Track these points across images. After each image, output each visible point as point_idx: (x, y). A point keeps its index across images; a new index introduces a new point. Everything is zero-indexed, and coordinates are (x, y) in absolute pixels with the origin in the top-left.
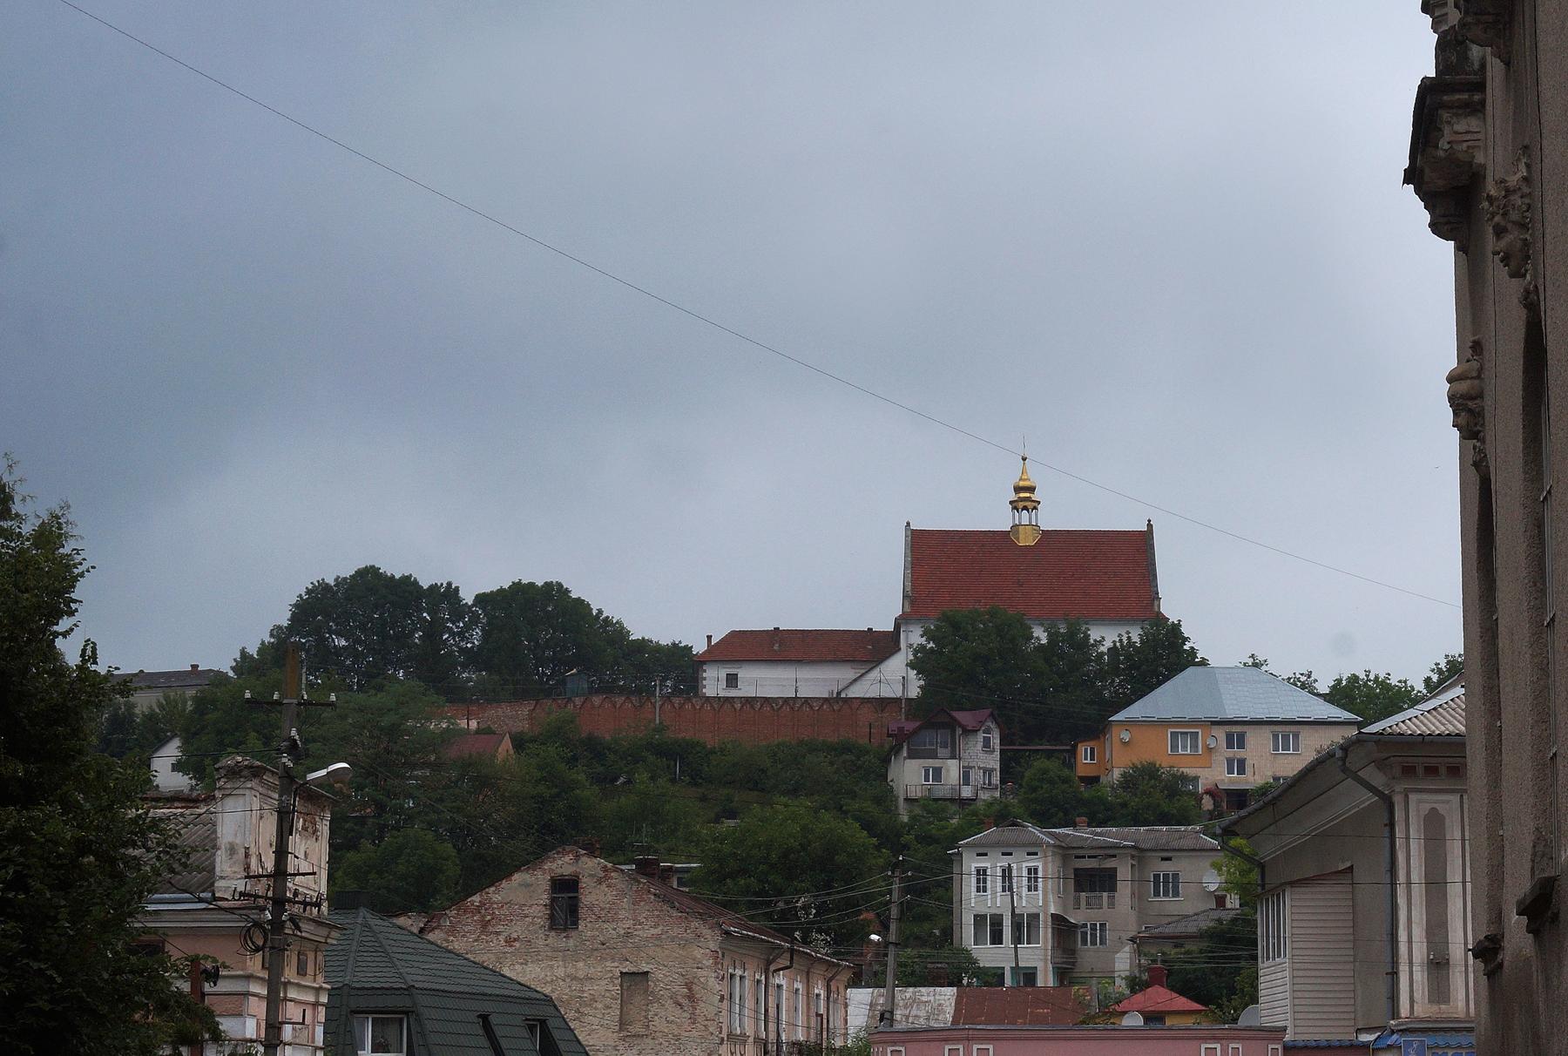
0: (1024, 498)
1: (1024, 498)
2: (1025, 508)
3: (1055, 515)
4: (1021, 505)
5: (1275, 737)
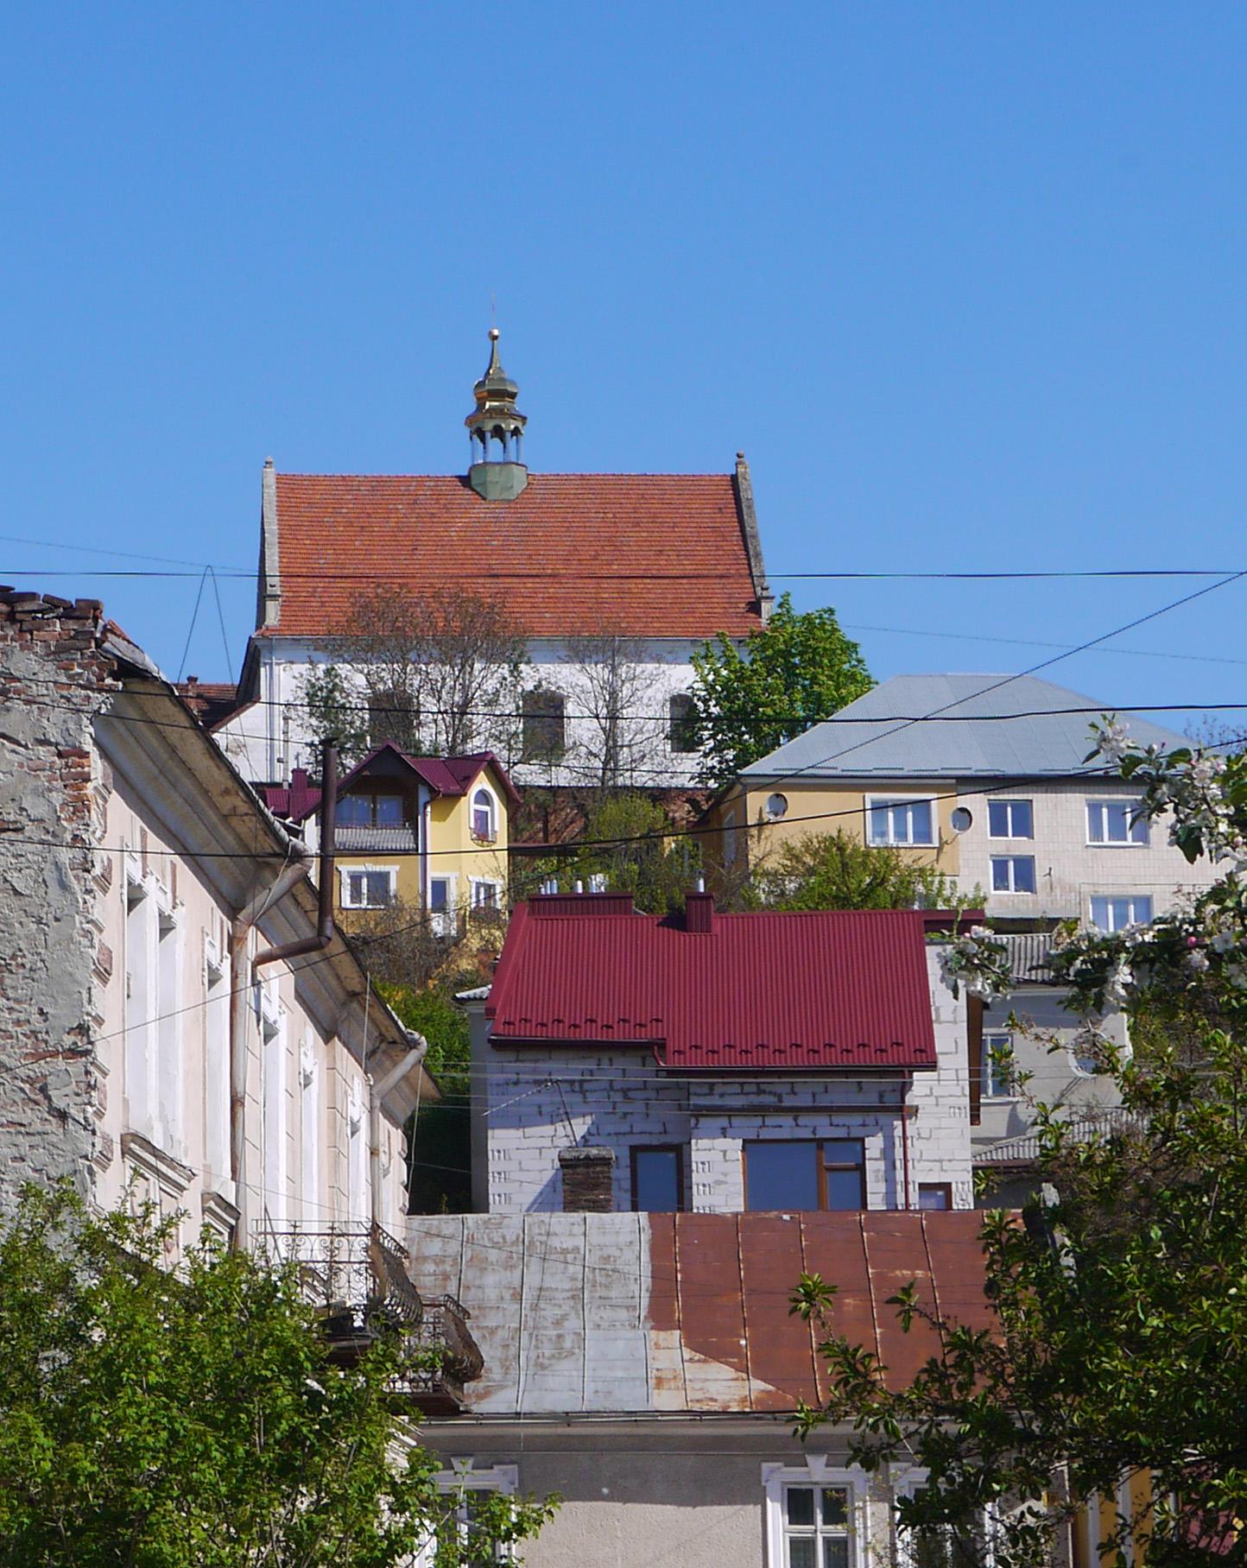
0: (494, 410)
1: (494, 410)
2: (498, 432)
3: (558, 443)
4: (489, 426)
5: (1095, 808)
